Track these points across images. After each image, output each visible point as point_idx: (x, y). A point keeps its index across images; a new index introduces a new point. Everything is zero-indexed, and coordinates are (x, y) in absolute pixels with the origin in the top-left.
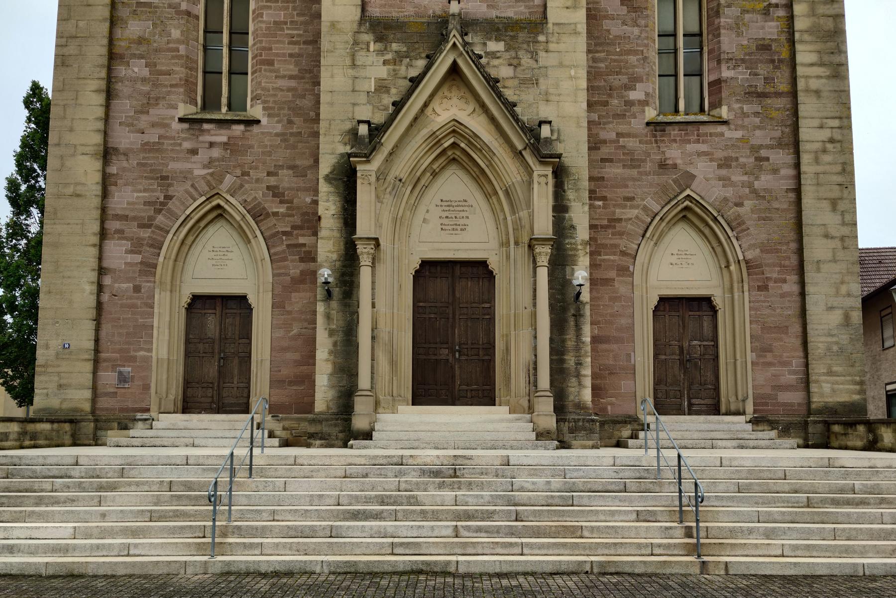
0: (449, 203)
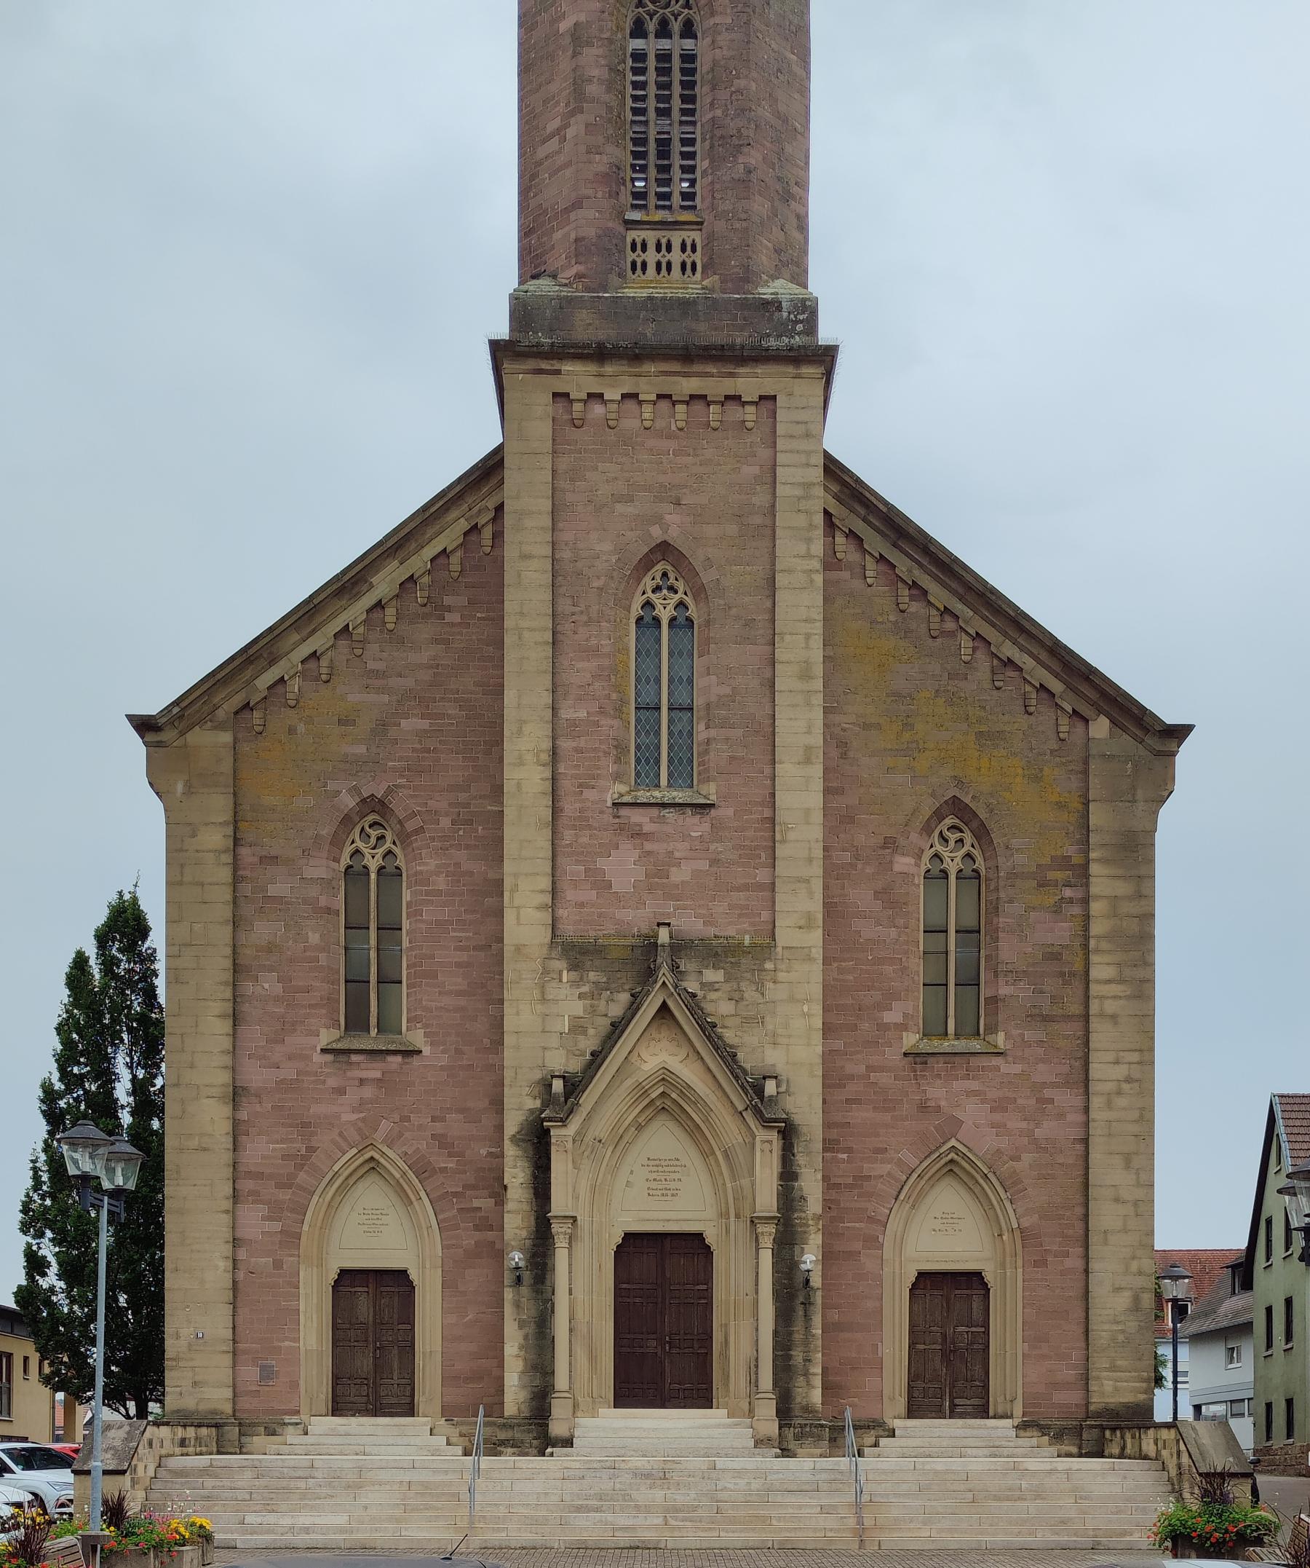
0: (658, 1162)
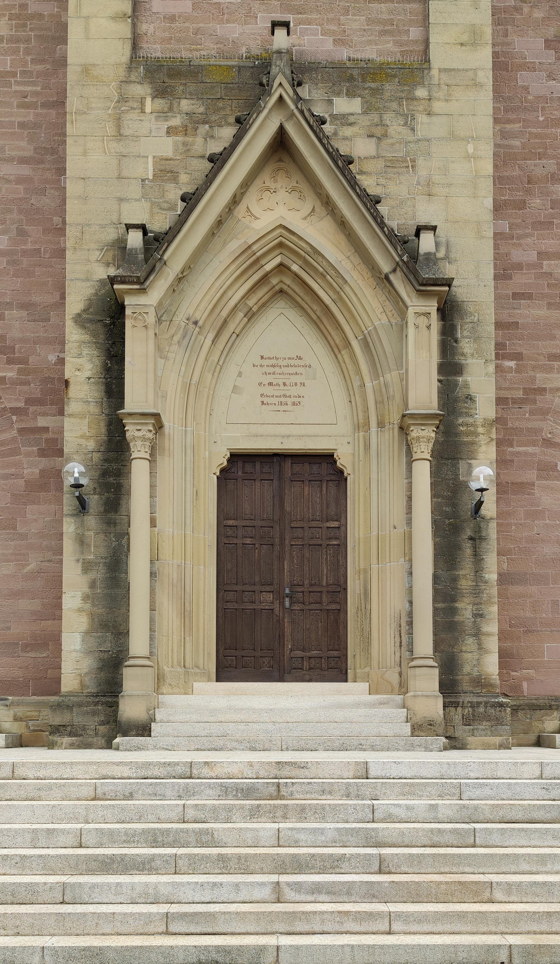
0: (274, 362)
